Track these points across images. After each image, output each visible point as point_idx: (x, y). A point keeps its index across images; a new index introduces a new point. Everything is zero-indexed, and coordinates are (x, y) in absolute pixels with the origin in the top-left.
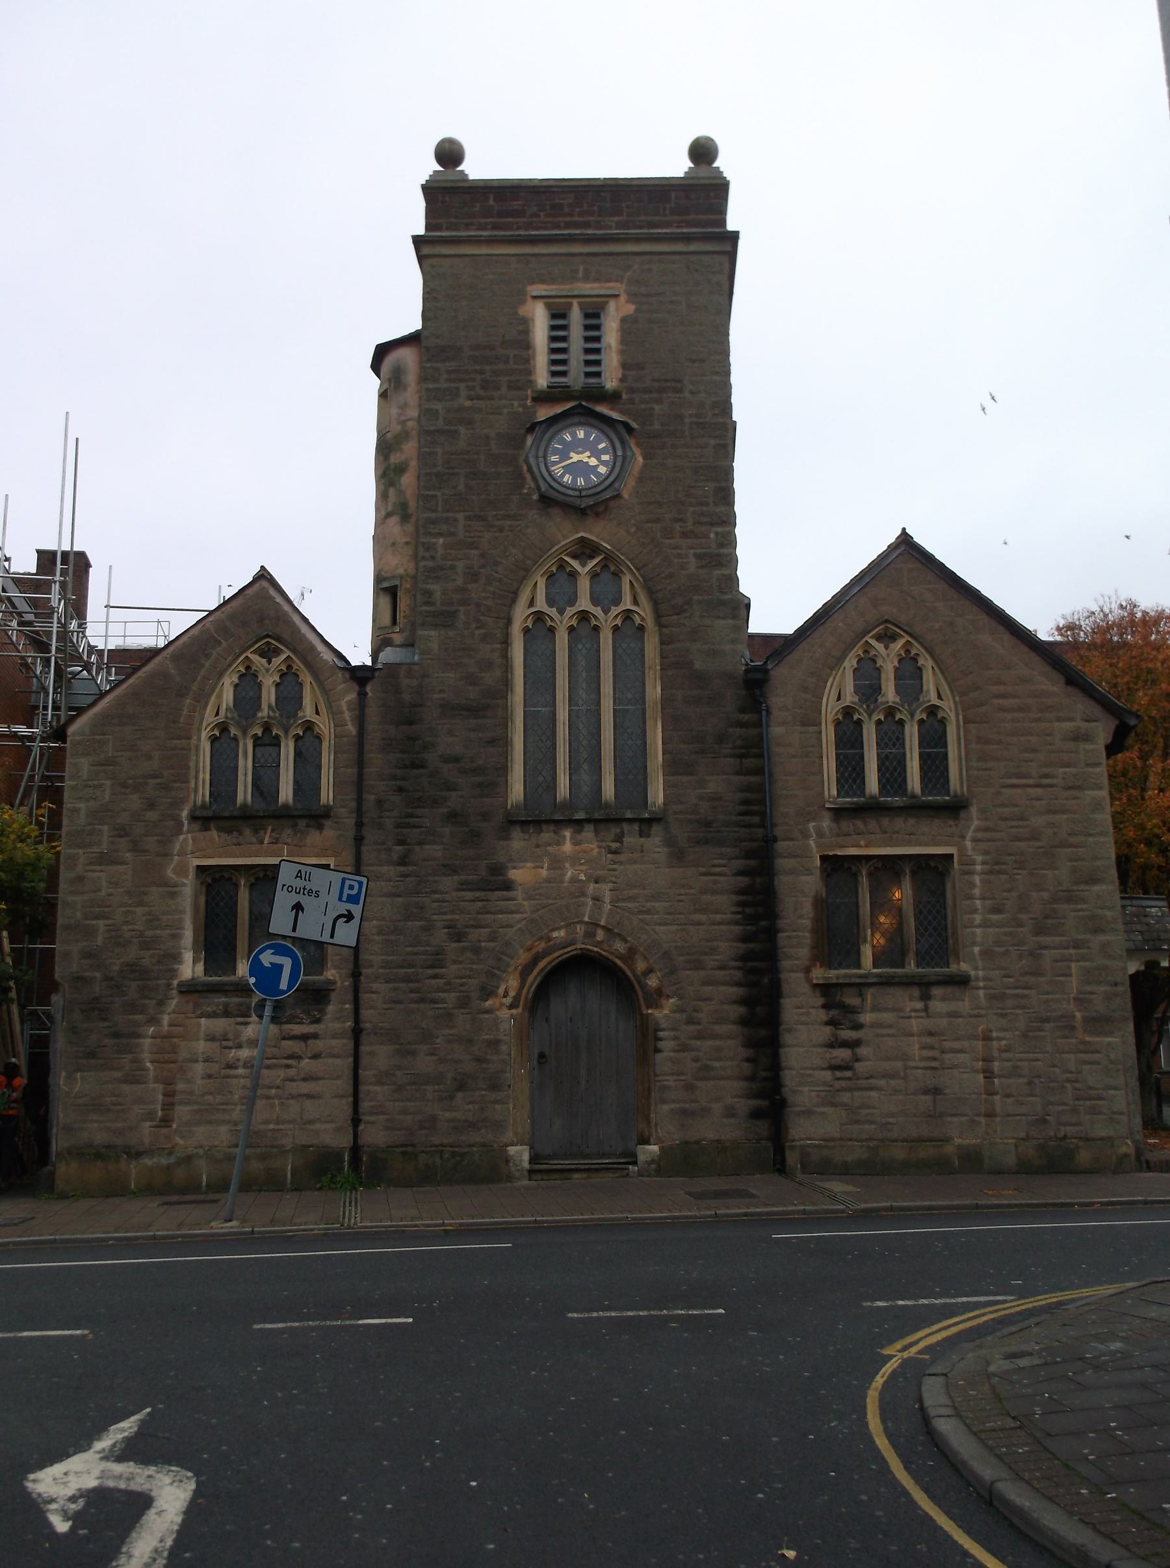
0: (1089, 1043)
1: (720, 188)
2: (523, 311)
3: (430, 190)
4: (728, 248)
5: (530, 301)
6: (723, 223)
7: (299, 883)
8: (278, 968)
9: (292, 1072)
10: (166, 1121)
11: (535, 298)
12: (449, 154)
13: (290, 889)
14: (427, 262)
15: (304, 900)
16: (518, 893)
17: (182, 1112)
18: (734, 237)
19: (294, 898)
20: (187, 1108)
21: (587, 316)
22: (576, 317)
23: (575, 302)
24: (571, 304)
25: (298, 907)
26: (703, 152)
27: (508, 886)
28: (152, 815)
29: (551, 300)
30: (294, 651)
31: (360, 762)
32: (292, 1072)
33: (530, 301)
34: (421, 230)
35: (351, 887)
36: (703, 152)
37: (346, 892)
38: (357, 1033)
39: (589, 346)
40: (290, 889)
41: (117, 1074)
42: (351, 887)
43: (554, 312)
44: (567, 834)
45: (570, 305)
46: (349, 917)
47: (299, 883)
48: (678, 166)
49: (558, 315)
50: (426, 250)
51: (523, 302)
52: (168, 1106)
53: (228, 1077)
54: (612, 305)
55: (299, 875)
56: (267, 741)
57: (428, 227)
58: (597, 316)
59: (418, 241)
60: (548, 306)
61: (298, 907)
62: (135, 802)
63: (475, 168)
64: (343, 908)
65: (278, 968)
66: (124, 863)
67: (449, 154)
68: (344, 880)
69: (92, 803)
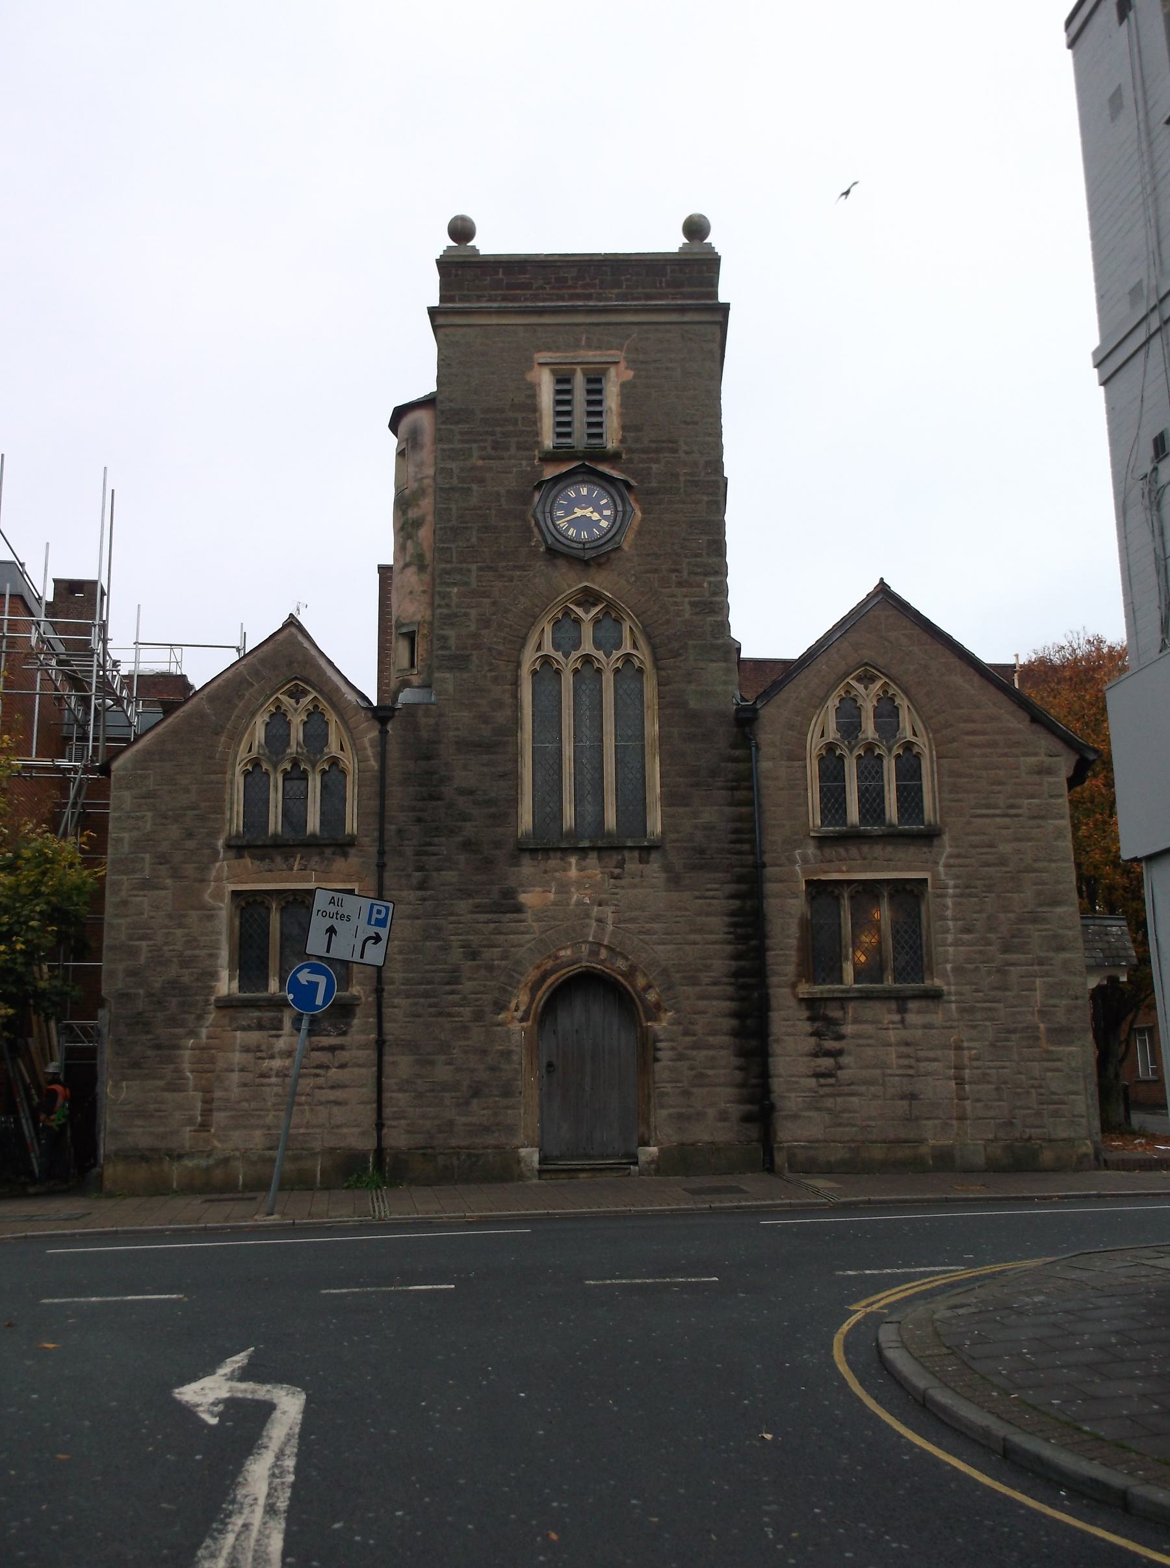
0: (1052, 1052)
1: (712, 263)
2: (530, 377)
3: (445, 265)
4: (719, 318)
5: (536, 367)
6: (715, 295)
7: (332, 909)
8: (314, 986)
9: (321, 1081)
10: (204, 1126)
11: (540, 364)
12: (461, 230)
13: (324, 914)
14: (441, 331)
15: (338, 925)
16: (528, 915)
17: (220, 1117)
18: (725, 308)
19: (328, 923)
20: (223, 1114)
21: (589, 381)
22: (579, 382)
23: (579, 369)
24: (575, 370)
25: (331, 931)
26: (696, 228)
27: (518, 909)
28: (191, 844)
29: (553, 367)
30: (320, 692)
31: (382, 795)
32: (321, 1081)
33: (536, 367)
34: (435, 302)
35: (379, 912)
36: (696, 228)
37: (375, 916)
38: (380, 1044)
39: (592, 409)
40: (324, 914)
41: (161, 1083)
42: (379, 912)
43: (559, 377)
44: (573, 860)
45: (574, 372)
46: (377, 939)
47: (332, 909)
48: (672, 242)
49: (563, 380)
50: (441, 320)
51: (531, 368)
52: (207, 1112)
53: (263, 1085)
54: (613, 372)
55: (332, 901)
56: (295, 775)
57: (441, 301)
58: (599, 381)
59: (432, 312)
60: (554, 372)
61: (331, 931)
62: (174, 831)
63: (486, 244)
64: (372, 931)
65: (314, 986)
66: (165, 888)
67: (461, 230)
68: (372, 905)
69: (135, 833)
